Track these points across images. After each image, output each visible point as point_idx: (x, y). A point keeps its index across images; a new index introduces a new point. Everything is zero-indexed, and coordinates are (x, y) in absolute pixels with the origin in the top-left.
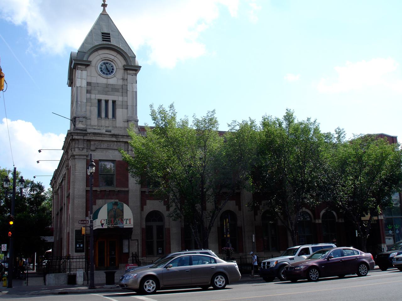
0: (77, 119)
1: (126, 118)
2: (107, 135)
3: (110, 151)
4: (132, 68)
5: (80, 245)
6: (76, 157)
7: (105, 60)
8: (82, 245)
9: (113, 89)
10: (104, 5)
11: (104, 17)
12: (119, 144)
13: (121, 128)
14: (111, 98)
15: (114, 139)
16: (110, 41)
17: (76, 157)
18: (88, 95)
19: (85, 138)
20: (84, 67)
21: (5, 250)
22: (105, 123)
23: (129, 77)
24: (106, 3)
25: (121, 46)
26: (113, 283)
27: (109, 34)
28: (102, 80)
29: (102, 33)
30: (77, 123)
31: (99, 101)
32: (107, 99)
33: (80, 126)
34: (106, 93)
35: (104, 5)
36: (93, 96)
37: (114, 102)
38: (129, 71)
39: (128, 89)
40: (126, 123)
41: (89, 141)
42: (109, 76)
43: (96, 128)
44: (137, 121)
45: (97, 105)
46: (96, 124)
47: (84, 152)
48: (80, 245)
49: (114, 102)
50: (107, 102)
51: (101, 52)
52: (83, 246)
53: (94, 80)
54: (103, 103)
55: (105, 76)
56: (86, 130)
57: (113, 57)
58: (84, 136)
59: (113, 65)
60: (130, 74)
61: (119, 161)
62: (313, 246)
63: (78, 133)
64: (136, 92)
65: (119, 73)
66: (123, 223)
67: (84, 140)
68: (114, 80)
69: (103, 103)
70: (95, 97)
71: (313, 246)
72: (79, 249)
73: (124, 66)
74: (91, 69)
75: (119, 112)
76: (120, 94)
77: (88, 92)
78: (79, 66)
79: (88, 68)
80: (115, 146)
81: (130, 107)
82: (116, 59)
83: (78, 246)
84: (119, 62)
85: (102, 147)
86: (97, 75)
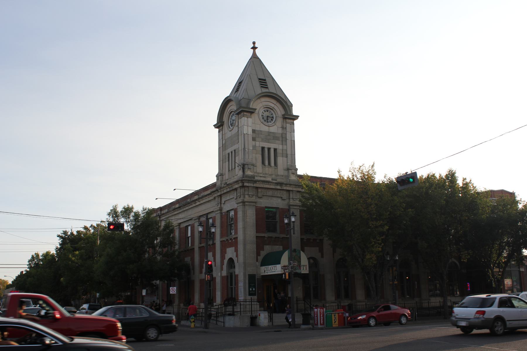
0: (246, 166)
1: (285, 167)
2: (271, 182)
3: (275, 199)
4: (290, 117)
5: (252, 289)
8: (254, 289)
9: (271, 137)
10: (254, 48)
11: (255, 62)
12: (282, 192)
13: (282, 176)
14: (272, 146)
15: (279, 187)
16: (267, 88)
17: (246, 204)
18: (254, 142)
19: (255, 185)
20: (249, 114)
22: (268, 170)
23: (288, 125)
24: (256, 46)
25: (279, 93)
26: (308, 324)
27: (265, 80)
29: (260, 79)
30: (246, 170)
31: (263, 148)
32: (269, 147)
33: (249, 173)
34: (267, 141)
35: (254, 48)
36: (258, 144)
37: (275, 150)
38: (287, 120)
39: (288, 138)
40: (286, 172)
41: (257, 188)
43: (261, 175)
44: (296, 170)
46: (261, 172)
47: (253, 199)
48: (252, 289)
49: (275, 150)
50: (269, 149)
51: (263, 99)
52: (168, 291)
53: (257, 128)
54: (266, 150)
55: (263, 121)
56: (254, 178)
57: (273, 105)
58: (253, 183)
60: (288, 123)
61: (282, 209)
63: (249, 180)
64: (294, 141)
65: (280, 122)
66: (300, 269)
67: (254, 187)
68: (275, 129)
69: (266, 150)
70: (260, 144)
72: (252, 292)
73: (283, 115)
74: (255, 116)
75: (280, 160)
76: (280, 142)
77: (254, 139)
78: (245, 113)
79: (253, 115)
80: (278, 194)
81: (289, 156)
82: (275, 107)
83: (251, 289)
84: (279, 111)
85: (268, 194)
86: (260, 123)
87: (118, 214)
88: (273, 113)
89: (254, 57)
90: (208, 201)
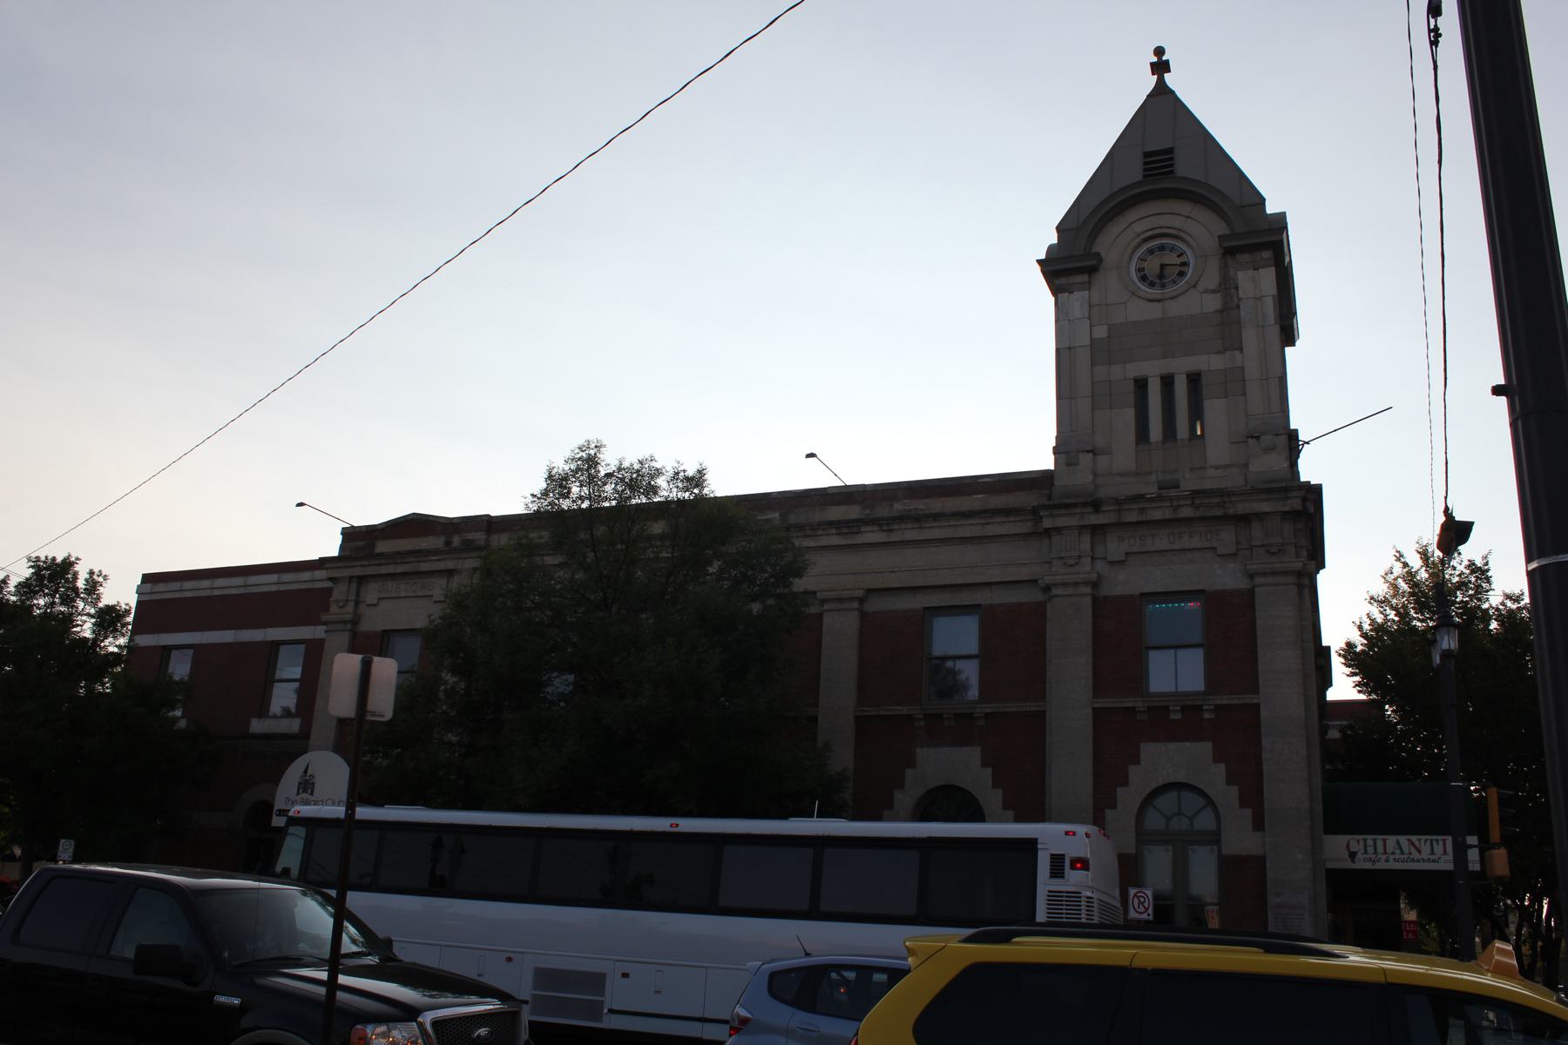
6: (1055, 591)
7: (1139, 245)
10: (1160, 67)
20: (1085, 278)
21: (1145, 916)
28: (1139, 311)
35: (1160, 67)
42: (1170, 290)
45: (1131, 399)
49: (1194, 379)
50: (1167, 382)
54: (1181, 387)
55: (1155, 292)
59: (1184, 247)
62: (52, 866)
69: (1181, 387)
71: (52, 866)
75: (1214, 408)
82: (1177, 222)
87: (345, 638)
88: (1184, 247)
89: (1161, 92)
90: (392, 576)
